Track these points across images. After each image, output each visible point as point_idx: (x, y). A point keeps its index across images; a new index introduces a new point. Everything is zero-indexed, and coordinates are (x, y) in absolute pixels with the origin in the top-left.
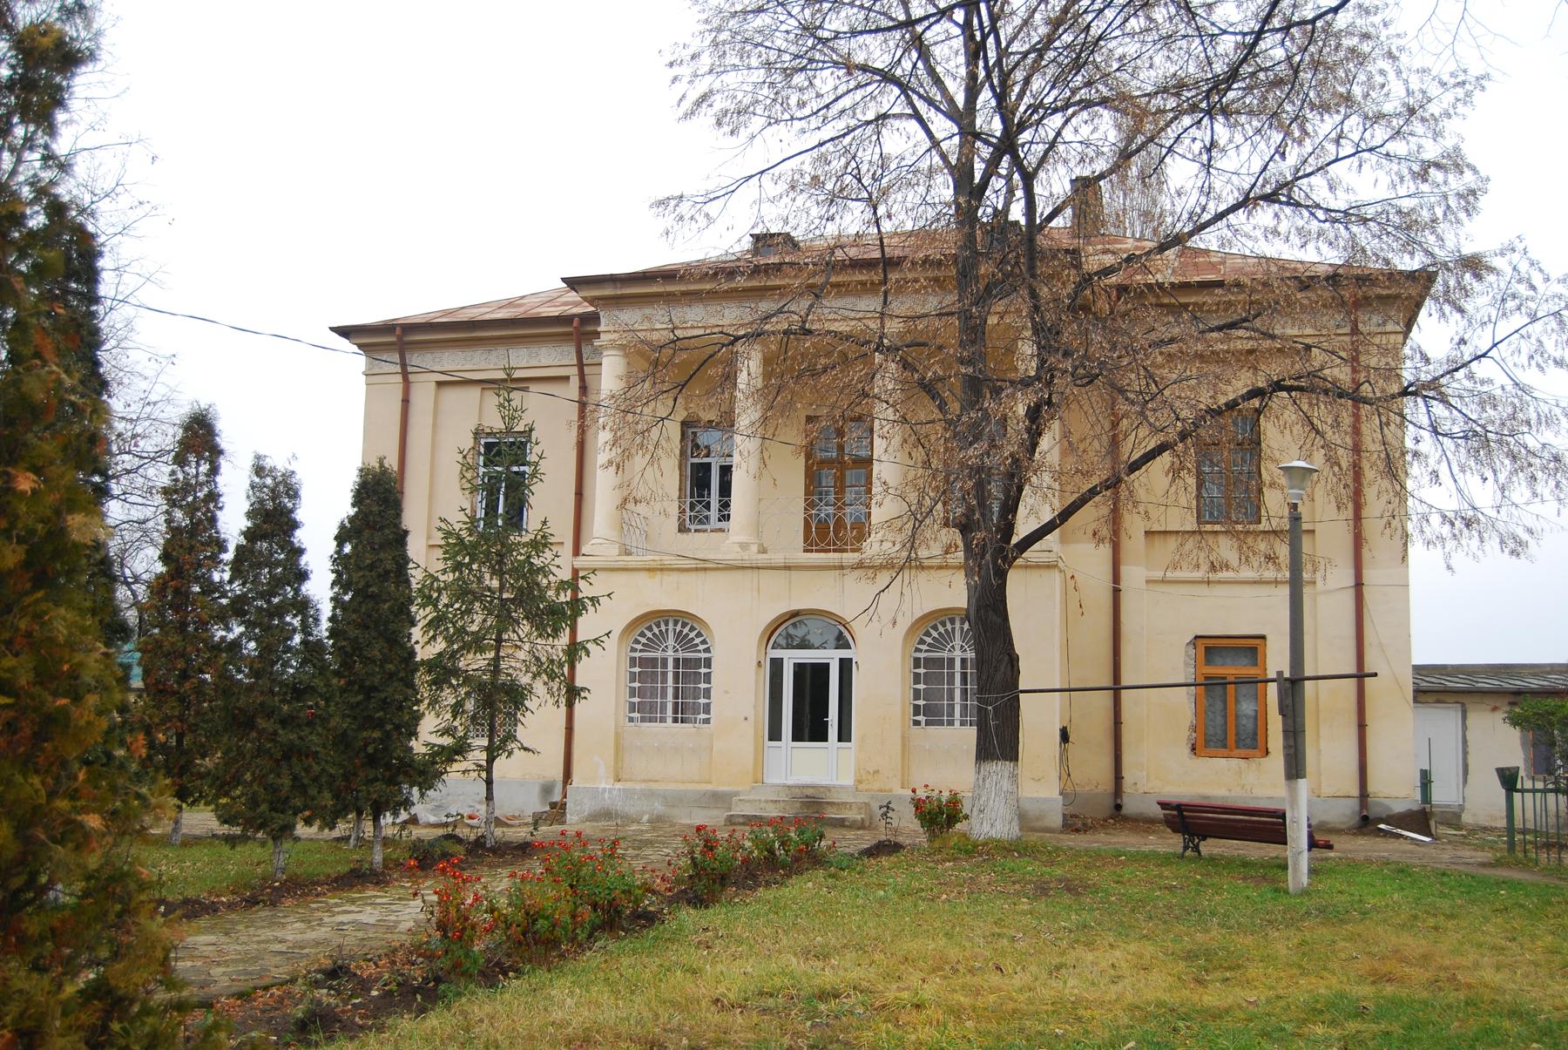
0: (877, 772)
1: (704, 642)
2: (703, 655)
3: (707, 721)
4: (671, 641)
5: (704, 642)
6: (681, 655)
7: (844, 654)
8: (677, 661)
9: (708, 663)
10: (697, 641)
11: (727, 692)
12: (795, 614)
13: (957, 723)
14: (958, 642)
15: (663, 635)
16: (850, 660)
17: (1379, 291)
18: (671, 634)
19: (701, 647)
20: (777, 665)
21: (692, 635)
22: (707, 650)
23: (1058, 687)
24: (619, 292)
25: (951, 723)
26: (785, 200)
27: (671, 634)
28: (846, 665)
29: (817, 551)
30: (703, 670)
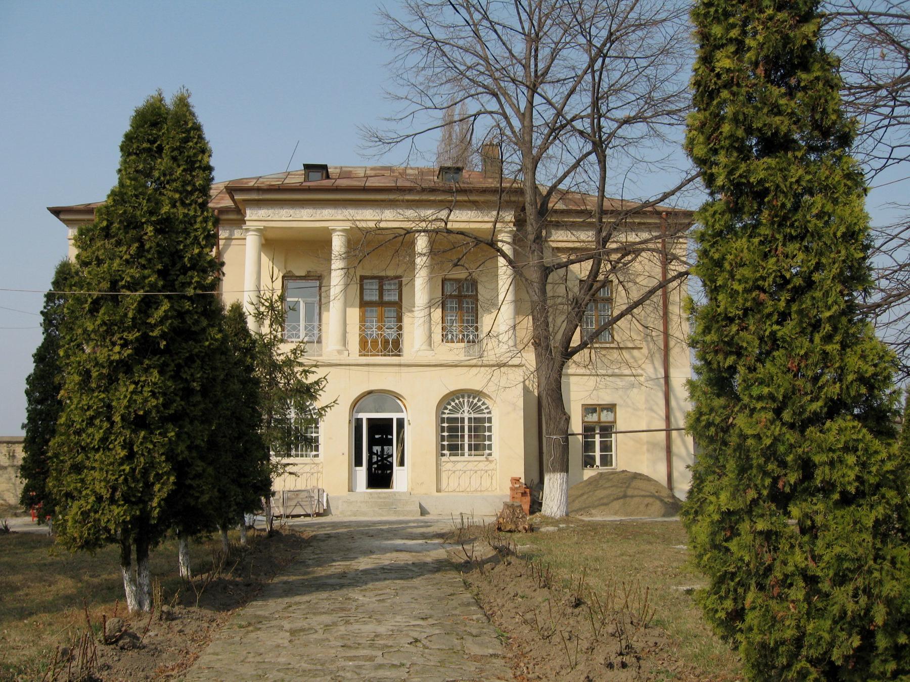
0: (422, 483)
1: (487, 408)
2: (487, 416)
3: (490, 455)
4: (466, 408)
5: (487, 408)
6: (473, 416)
7: (400, 415)
8: (470, 419)
9: (490, 420)
10: (483, 407)
11: (331, 438)
12: (370, 392)
13: (466, 454)
14: (466, 408)
15: (462, 404)
16: (403, 419)
17: (780, 248)
18: (466, 404)
19: (485, 411)
20: (359, 422)
21: (479, 404)
22: (489, 413)
23: (645, 429)
24: (261, 197)
25: (463, 455)
26: (376, 158)
27: (466, 404)
28: (401, 423)
29: (371, 355)
30: (487, 425)
